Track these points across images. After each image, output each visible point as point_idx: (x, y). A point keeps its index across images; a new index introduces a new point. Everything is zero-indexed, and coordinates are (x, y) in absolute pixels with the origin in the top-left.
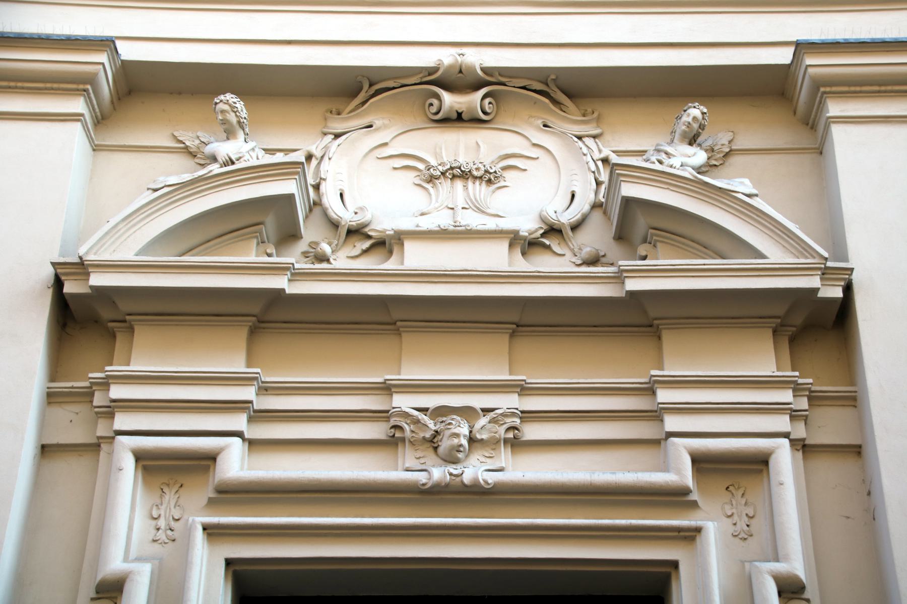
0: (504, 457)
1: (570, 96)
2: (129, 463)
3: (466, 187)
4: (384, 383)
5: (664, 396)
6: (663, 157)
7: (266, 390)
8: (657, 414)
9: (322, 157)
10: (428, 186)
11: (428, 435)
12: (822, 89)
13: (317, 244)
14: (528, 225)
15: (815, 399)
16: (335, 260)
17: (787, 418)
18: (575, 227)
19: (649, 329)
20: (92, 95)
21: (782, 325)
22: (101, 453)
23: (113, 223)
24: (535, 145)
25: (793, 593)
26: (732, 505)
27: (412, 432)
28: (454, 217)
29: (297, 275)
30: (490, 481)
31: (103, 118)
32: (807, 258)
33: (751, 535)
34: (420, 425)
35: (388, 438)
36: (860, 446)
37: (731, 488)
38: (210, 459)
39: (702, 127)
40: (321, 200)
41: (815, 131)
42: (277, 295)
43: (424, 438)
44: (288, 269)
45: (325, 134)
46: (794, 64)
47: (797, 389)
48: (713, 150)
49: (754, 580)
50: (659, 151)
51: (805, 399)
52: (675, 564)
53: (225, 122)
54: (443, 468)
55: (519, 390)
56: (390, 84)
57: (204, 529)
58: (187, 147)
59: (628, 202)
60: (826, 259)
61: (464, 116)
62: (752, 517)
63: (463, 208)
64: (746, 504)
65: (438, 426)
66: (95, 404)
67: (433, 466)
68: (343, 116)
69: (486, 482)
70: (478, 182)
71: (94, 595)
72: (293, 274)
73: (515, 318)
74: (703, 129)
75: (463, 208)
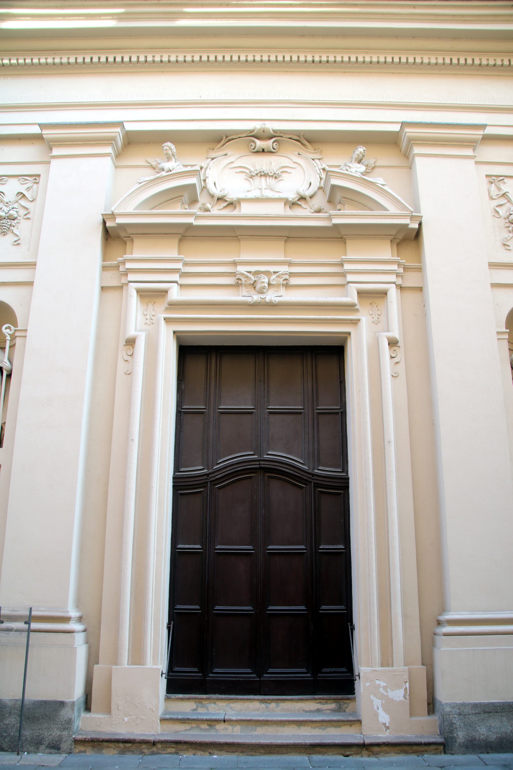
0: (282, 291)
1: (309, 142)
2: (134, 293)
3: (266, 180)
4: (234, 261)
5: (347, 267)
6: (348, 168)
7: (186, 264)
8: (344, 274)
9: (207, 168)
10: (251, 180)
11: (252, 282)
12: (412, 142)
13: (205, 204)
14: (292, 196)
15: (405, 269)
16: (212, 210)
17: (395, 276)
18: (311, 197)
19: (341, 239)
20: (114, 145)
21: (394, 239)
22: (124, 290)
23: (124, 197)
24: (295, 162)
25: (394, 344)
26: (372, 310)
27: (245, 281)
28: (261, 193)
29: (197, 217)
30: (277, 301)
31: (119, 155)
32: (405, 211)
33: (379, 322)
34: (248, 278)
35: (235, 284)
36: (422, 288)
37: (372, 304)
38: (165, 292)
39: (363, 156)
40: (206, 186)
41: (409, 159)
42: (189, 226)
43: (250, 284)
44: (194, 214)
45: (208, 158)
46: (401, 131)
47: (399, 264)
48: (368, 166)
49: (379, 340)
50: (346, 165)
51: (402, 269)
52: (349, 334)
53: (167, 154)
54: (258, 296)
55: (288, 264)
56: (234, 137)
57: (164, 319)
58: (152, 165)
59: (333, 187)
60: (412, 212)
61: (265, 150)
62: (380, 315)
63: (265, 189)
64: (378, 310)
65: (256, 279)
66: (120, 270)
67: (254, 295)
68: (215, 150)
69: (275, 301)
70: (271, 178)
71: (125, 344)
72: (196, 217)
73: (287, 235)
74: (364, 157)
75: (265, 189)
